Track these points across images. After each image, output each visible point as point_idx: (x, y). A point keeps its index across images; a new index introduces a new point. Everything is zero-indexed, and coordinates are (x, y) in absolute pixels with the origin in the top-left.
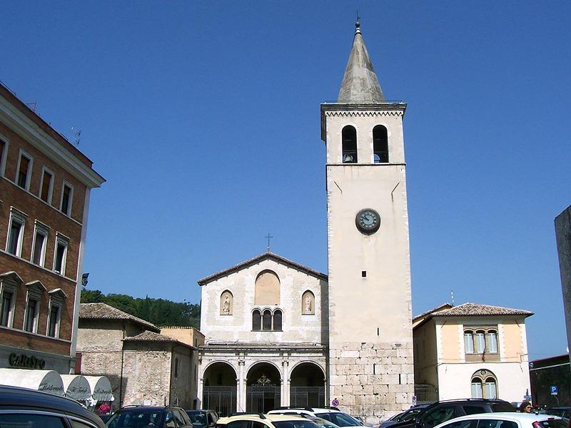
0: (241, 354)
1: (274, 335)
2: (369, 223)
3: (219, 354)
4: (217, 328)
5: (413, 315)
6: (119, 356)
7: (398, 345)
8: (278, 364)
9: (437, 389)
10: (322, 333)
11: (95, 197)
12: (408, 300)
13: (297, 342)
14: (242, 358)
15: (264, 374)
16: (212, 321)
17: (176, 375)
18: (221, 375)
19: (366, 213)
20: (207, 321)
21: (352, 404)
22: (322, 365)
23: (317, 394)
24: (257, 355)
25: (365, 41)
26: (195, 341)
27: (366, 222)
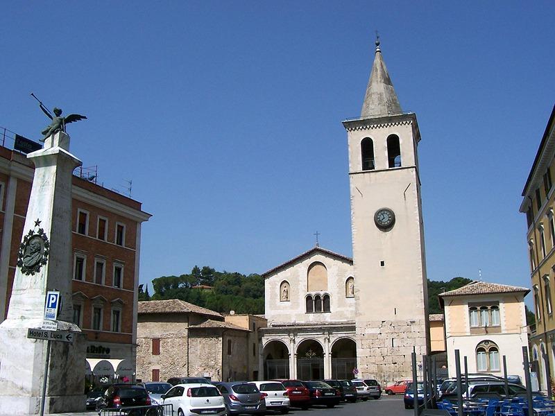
2: (386, 221)
6: (185, 340)
7: (414, 322)
11: (145, 228)
16: (274, 307)
17: (229, 353)
18: (279, 350)
20: (270, 307)
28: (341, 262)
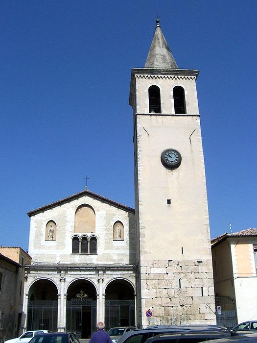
0: (62, 272)
1: (90, 258)
2: (172, 160)
3: (43, 272)
4: (42, 251)
5: (211, 239)
7: (200, 262)
8: (94, 281)
9: (234, 300)
10: (130, 256)
12: (206, 223)
13: (109, 263)
14: (63, 276)
15: (82, 290)
16: (38, 245)
19: (170, 152)
20: (35, 246)
21: (161, 315)
22: (133, 281)
23: (128, 307)
24: (76, 273)
25: (163, 31)
26: (22, 260)
27: (169, 159)
28: (109, 205)
